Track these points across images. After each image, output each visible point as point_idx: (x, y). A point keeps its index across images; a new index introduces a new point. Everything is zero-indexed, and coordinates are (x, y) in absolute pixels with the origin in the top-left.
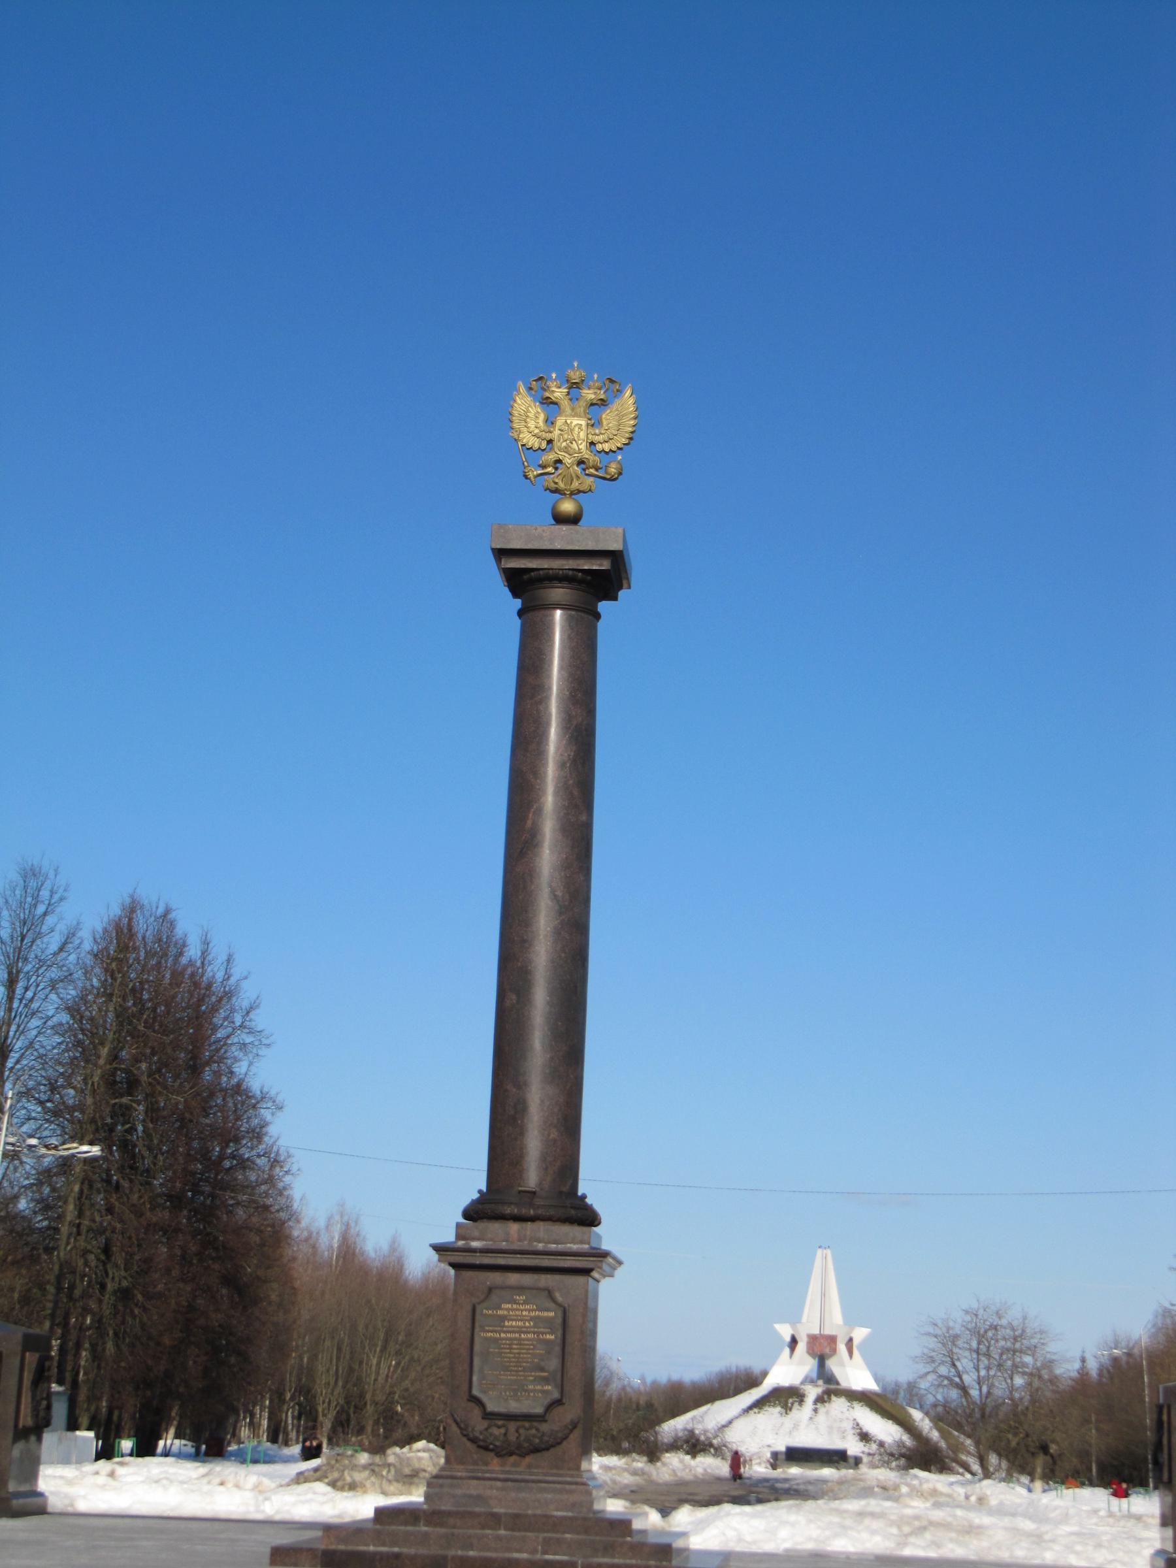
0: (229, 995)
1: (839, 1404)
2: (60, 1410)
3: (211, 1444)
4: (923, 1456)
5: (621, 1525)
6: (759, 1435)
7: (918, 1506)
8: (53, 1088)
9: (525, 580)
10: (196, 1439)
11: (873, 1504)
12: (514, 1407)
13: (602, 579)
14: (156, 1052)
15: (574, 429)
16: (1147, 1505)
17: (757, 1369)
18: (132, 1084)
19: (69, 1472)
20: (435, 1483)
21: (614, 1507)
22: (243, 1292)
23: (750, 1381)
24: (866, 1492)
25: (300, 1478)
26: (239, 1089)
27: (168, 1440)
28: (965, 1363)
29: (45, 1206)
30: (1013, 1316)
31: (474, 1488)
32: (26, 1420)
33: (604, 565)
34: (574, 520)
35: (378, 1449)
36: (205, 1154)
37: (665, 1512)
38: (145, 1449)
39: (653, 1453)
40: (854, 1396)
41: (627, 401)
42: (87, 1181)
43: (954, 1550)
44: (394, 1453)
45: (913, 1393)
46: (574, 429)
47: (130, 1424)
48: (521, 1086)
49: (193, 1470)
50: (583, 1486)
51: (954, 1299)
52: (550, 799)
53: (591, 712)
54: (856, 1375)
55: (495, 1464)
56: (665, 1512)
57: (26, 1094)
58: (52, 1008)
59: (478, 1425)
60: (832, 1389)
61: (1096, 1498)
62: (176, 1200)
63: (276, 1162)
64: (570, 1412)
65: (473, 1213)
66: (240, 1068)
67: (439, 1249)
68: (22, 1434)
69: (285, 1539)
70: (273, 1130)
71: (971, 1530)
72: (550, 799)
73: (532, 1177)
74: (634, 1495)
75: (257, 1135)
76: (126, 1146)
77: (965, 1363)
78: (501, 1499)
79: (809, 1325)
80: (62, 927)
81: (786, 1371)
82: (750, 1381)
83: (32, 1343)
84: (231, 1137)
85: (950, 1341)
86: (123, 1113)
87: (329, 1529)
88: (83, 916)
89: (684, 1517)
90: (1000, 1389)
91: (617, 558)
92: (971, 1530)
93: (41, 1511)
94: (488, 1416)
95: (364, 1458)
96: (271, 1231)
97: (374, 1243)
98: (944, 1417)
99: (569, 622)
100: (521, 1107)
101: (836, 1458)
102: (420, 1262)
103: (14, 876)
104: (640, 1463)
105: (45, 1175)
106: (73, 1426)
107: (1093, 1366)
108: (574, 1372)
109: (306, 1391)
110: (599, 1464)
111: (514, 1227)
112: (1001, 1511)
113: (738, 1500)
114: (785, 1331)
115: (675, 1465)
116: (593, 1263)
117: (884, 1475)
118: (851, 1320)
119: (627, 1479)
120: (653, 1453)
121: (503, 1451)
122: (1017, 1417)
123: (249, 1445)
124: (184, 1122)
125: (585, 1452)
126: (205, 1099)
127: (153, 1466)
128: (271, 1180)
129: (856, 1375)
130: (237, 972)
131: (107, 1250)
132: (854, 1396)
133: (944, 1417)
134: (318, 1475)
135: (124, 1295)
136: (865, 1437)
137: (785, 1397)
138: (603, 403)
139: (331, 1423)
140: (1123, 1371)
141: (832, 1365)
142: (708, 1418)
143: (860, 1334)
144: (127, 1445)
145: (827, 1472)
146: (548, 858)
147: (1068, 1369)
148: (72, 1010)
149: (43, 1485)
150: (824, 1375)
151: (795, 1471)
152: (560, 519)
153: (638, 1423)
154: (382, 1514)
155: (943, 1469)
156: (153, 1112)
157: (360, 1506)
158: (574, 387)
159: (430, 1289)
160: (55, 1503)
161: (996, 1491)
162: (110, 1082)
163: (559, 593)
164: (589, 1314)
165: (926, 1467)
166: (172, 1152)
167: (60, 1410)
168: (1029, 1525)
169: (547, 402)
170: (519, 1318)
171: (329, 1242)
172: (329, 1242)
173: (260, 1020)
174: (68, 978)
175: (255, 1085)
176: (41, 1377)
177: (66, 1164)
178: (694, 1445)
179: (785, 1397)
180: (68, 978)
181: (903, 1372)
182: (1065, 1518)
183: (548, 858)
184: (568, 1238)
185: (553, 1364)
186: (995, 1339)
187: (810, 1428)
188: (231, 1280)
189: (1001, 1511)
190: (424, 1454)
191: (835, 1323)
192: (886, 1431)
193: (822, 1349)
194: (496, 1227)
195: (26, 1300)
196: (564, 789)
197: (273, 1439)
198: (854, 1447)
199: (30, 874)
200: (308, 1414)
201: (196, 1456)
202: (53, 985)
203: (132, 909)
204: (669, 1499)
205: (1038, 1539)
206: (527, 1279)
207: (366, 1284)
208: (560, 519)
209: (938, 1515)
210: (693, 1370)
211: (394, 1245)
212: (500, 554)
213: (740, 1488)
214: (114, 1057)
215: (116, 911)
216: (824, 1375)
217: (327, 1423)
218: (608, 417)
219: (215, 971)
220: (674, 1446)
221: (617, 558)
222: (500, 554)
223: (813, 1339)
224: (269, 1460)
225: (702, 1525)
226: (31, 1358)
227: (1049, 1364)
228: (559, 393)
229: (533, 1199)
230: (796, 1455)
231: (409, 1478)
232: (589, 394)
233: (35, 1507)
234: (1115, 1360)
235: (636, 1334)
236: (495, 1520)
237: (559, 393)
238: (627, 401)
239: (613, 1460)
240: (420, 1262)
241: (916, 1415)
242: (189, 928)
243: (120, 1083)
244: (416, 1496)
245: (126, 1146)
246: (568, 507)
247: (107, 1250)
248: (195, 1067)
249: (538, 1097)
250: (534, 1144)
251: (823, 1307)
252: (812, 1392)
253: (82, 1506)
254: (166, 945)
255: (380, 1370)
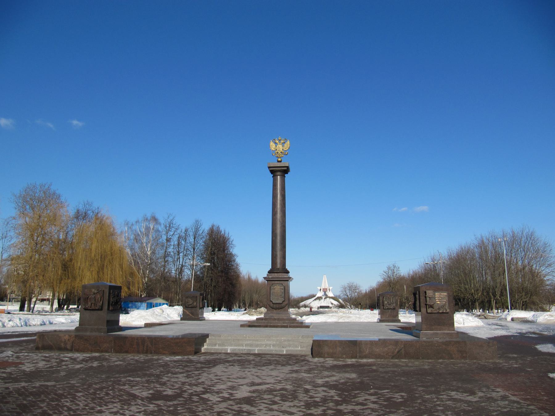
0: (229, 239)
1: (328, 299)
2: (206, 304)
3: (230, 309)
4: (341, 306)
5: (295, 319)
6: (315, 304)
7: (341, 314)
8: (202, 255)
9: (273, 171)
10: (227, 308)
11: (334, 314)
12: (277, 302)
13: (285, 171)
14: (217, 249)
15: (280, 147)
16: (376, 312)
17: (315, 294)
18: (214, 254)
19: (208, 314)
20: (265, 314)
21: (294, 316)
22: (233, 285)
23: (314, 296)
24: (333, 312)
25: (244, 314)
26: (231, 254)
27: (223, 309)
28: (348, 292)
29: (202, 273)
30: (355, 284)
31: (271, 315)
32: (201, 306)
33: (286, 168)
34: (281, 161)
35: (256, 309)
36: (226, 264)
37: (301, 317)
38: (219, 310)
39: (299, 308)
40: (330, 298)
41: (288, 142)
42: (208, 269)
43: (347, 320)
44: (258, 310)
45: (339, 297)
46: (280, 147)
47: (217, 306)
48: (276, 252)
49: (227, 313)
50: (289, 314)
51: (346, 281)
52: (279, 206)
53: (285, 192)
54: (330, 294)
55: (275, 311)
56: (301, 317)
57: (198, 256)
58: (201, 242)
59: (272, 305)
60: (327, 297)
61: (368, 311)
62: (222, 272)
63: (237, 265)
64: (286, 302)
65: (270, 272)
66: (231, 251)
67: (264, 278)
68: (201, 308)
69: (243, 323)
70: (237, 260)
71: (349, 317)
72: (279, 206)
73: (279, 266)
74: (296, 314)
75: (234, 261)
76: (214, 263)
77: (348, 292)
78: (276, 316)
79: (323, 287)
80: (202, 229)
81: (320, 294)
82: (314, 296)
83: (201, 294)
84: (230, 261)
85: (345, 289)
86: (213, 258)
87: (249, 321)
88: (205, 227)
89: (304, 318)
90: (353, 295)
91: (288, 167)
92: (349, 317)
93: (204, 320)
94: (273, 303)
95: (254, 310)
96: (237, 276)
97: (253, 277)
98: (344, 300)
99: (281, 178)
100: (276, 255)
101: (328, 307)
102: (261, 279)
103: (194, 222)
104: (297, 309)
105: (201, 268)
106: (208, 307)
107: (367, 291)
108: (286, 296)
109: (244, 300)
110: (291, 310)
111: (276, 274)
112: (354, 314)
113: (313, 315)
114: (319, 288)
115: (303, 310)
116: (288, 279)
117: (336, 309)
118: (329, 286)
119: (295, 312)
120: (299, 308)
121: (276, 309)
122: (356, 300)
123: (236, 309)
124: (223, 259)
125: (289, 308)
126: (226, 256)
127: (221, 312)
128: (237, 268)
129: (330, 294)
130: (230, 236)
131: (212, 280)
132: (330, 298)
133: (344, 300)
134: (247, 313)
135: (215, 286)
136: (332, 304)
137: (319, 298)
138: (284, 143)
139: (250, 305)
140: (372, 292)
141: (327, 293)
142: (307, 302)
143: (331, 288)
144: (217, 309)
145: (326, 309)
146: (279, 215)
147: (364, 292)
148: (204, 242)
149: (204, 316)
150: (325, 294)
151: (321, 309)
152: (278, 162)
153: (296, 303)
154: (257, 319)
155: (345, 308)
156: (218, 258)
157: (254, 318)
158: (280, 140)
159: (263, 284)
160: (206, 319)
161: (353, 311)
162: (211, 253)
163: (279, 173)
164: (288, 287)
165: (342, 308)
166: (221, 264)
167: (206, 304)
168: (358, 316)
169: (275, 143)
170: (277, 288)
171: (246, 277)
172: (246, 277)
173: (234, 243)
174: (203, 237)
175: (233, 253)
176: (203, 300)
177: (205, 266)
178: (305, 306)
179: (319, 298)
180: (203, 237)
181: (338, 293)
182: (364, 314)
183: (279, 215)
184: (285, 275)
185: (283, 295)
186: (352, 288)
187: (323, 303)
188: (231, 284)
189: (354, 314)
190: (263, 310)
191: (327, 286)
192: (336, 303)
193: (325, 291)
194: (273, 274)
195: (200, 288)
196: (281, 204)
197: (239, 308)
198: (330, 305)
199: (197, 221)
200: (244, 304)
201: (227, 311)
202: (201, 239)
203: (213, 226)
204: (302, 315)
205: (359, 318)
206: (278, 282)
207: (253, 284)
208: (278, 162)
209: (344, 315)
210: (305, 295)
211: (257, 277)
212: (269, 167)
213: (312, 313)
214: (211, 249)
215: (210, 226)
216: (325, 294)
217: (247, 305)
218: (285, 145)
219: (226, 235)
220: (302, 307)
221: (288, 167)
222: (269, 167)
223: (323, 289)
224: (239, 311)
225: (307, 319)
226: (201, 297)
227: (361, 291)
228: (277, 142)
229: (279, 270)
230: (321, 307)
231: (261, 313)
232: (282, 142)
233: (203, 319)
234: (112, 234)
235: (296, 290)
236: (275, 319)
237: (277, 142)
238: (288, 142)
239: (293, 309)
240: (261, 279)
241: (340, 300)
242: (222, 228)
243: (212, 254)
244: (262, 316)
245: (214, 263)
246: (279, 159)
247: (212, 280)
248: (224, 251)
249: (279, 254)
250: (279, 261)
251: (325, 284)
252: (324, 297)
253: (210, 319)
254: (219, 232)
255: (255, 297)
